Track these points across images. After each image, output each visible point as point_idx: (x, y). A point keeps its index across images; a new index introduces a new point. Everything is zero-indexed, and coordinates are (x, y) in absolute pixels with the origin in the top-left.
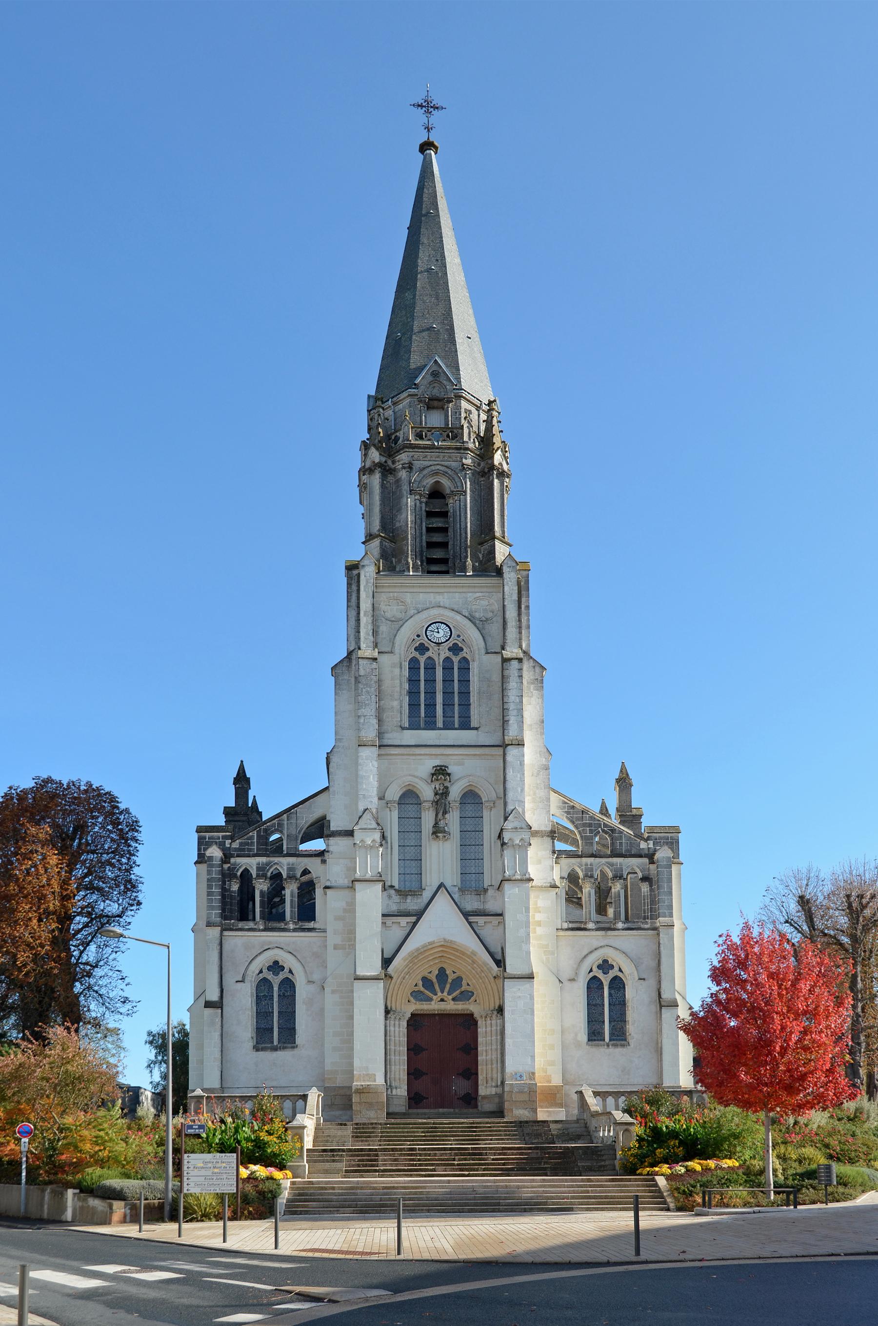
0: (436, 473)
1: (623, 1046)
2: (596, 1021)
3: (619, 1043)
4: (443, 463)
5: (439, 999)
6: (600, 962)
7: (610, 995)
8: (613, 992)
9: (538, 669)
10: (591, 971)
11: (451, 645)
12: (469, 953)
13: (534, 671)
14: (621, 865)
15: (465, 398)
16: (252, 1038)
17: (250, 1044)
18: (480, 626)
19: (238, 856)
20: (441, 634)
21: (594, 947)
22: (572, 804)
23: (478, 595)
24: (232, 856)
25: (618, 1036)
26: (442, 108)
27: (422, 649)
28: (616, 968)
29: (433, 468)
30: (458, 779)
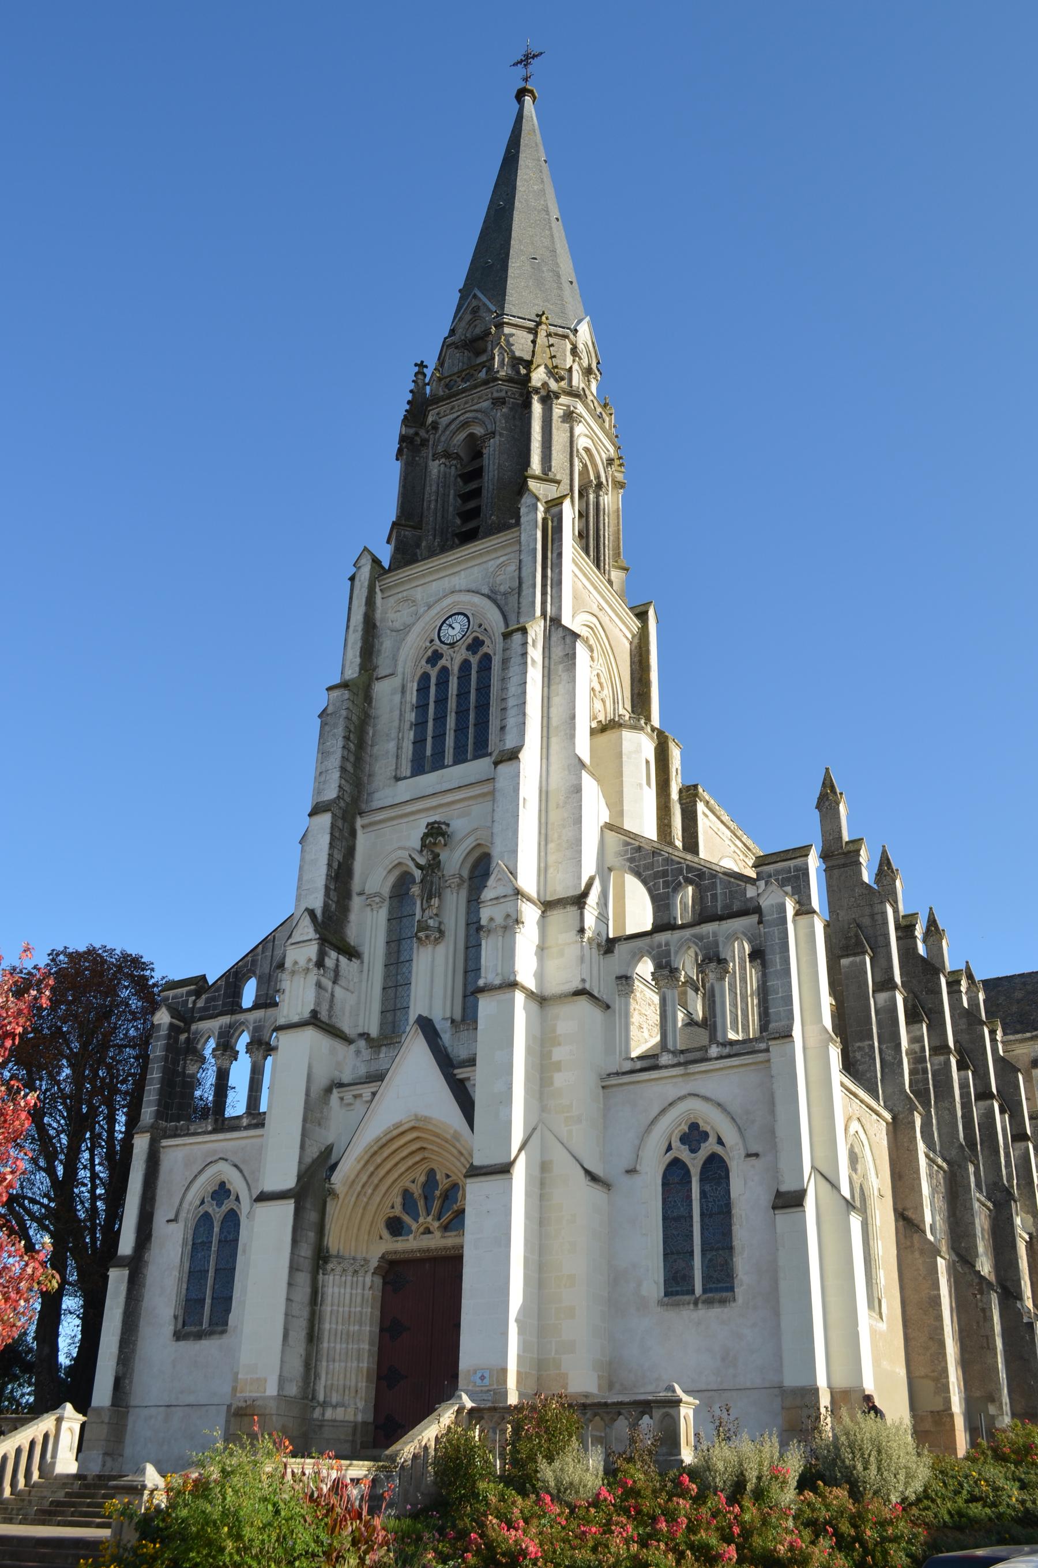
0: (465, 424)
1: (723, 1302)
2: (678, 1253)
3: (717, 1296)
4: (473, 408)
5: (421, 1230)
6: (685, 1128)
7: (703, 1194)
8: (707, 1188)
9: (568, 640)
10: (669, 1148)
11: (470, 640)
12: (449, 1137)
13: (565, 644)
14: (715, 934)
15: (508, 324)
16: (176, 1317)
17: (169, 1329)
18: (502, 603)
19: (201, 1019)
20: (455, 630)
21: (670, 1100)
22: (637, 843)
23: (502, 559)
24: (194, 1020)
25: (719, 1281)
26: (542, 53)
27: (435, 658)
28: (712, 1139)
29: (461, 418)
30: (461, 840)
